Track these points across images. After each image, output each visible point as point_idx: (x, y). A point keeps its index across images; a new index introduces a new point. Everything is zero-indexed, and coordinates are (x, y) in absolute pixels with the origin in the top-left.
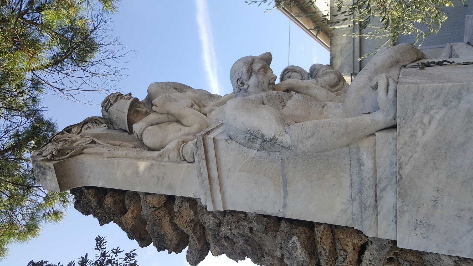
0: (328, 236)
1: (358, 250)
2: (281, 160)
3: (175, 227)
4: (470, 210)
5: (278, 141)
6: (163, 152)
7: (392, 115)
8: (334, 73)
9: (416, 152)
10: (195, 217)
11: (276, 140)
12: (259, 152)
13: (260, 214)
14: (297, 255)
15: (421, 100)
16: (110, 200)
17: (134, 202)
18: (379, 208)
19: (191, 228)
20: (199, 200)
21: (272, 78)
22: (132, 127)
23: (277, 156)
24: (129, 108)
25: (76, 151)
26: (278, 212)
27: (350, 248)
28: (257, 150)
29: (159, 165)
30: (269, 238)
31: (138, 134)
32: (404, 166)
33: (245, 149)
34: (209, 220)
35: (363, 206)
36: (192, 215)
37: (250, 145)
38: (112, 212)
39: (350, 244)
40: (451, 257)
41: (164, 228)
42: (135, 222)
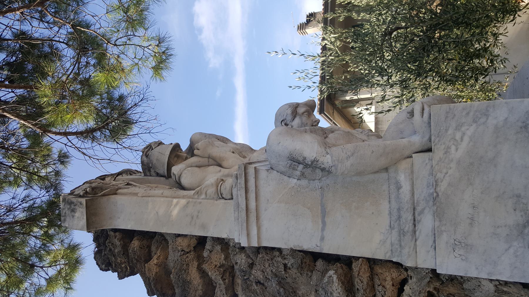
0: (367, 270)
1: (397, 286)
2: (321, 188)
3: (203, 273)
4: (505, 226)
5: (319, 162)
6: (201, 189)
7: (427, 138)
8: (376, 136)
9: (451, 168)
10: (225, 261)
11: (317, 161)
12: (299, 180)
13: (296, 250)
14: (332, 290)
15: (453, 118)
16: (137, 243)
17: (161, 248)
18: (417, 233)
19: (220, 274)
20: (232, 240)
21: (315, 121)
22: (171, 169)
23: (317, 185)
24: (171, 151)
25: (111, 190)
26: (315, 246)
27: (388, 284)
28: (298, 179)
29: (195, 203)
30: (304, 280)
31: (176, 175)
32: (440, 183)
33: (286, 178)
34: (242, 259)
35: (402, 233)
36: (223, 259)
37: (291, 173)
38: (136, 257)
39: (388, 279)
40: (491, 280)
41: (190, 275)
42: (159, 270)
